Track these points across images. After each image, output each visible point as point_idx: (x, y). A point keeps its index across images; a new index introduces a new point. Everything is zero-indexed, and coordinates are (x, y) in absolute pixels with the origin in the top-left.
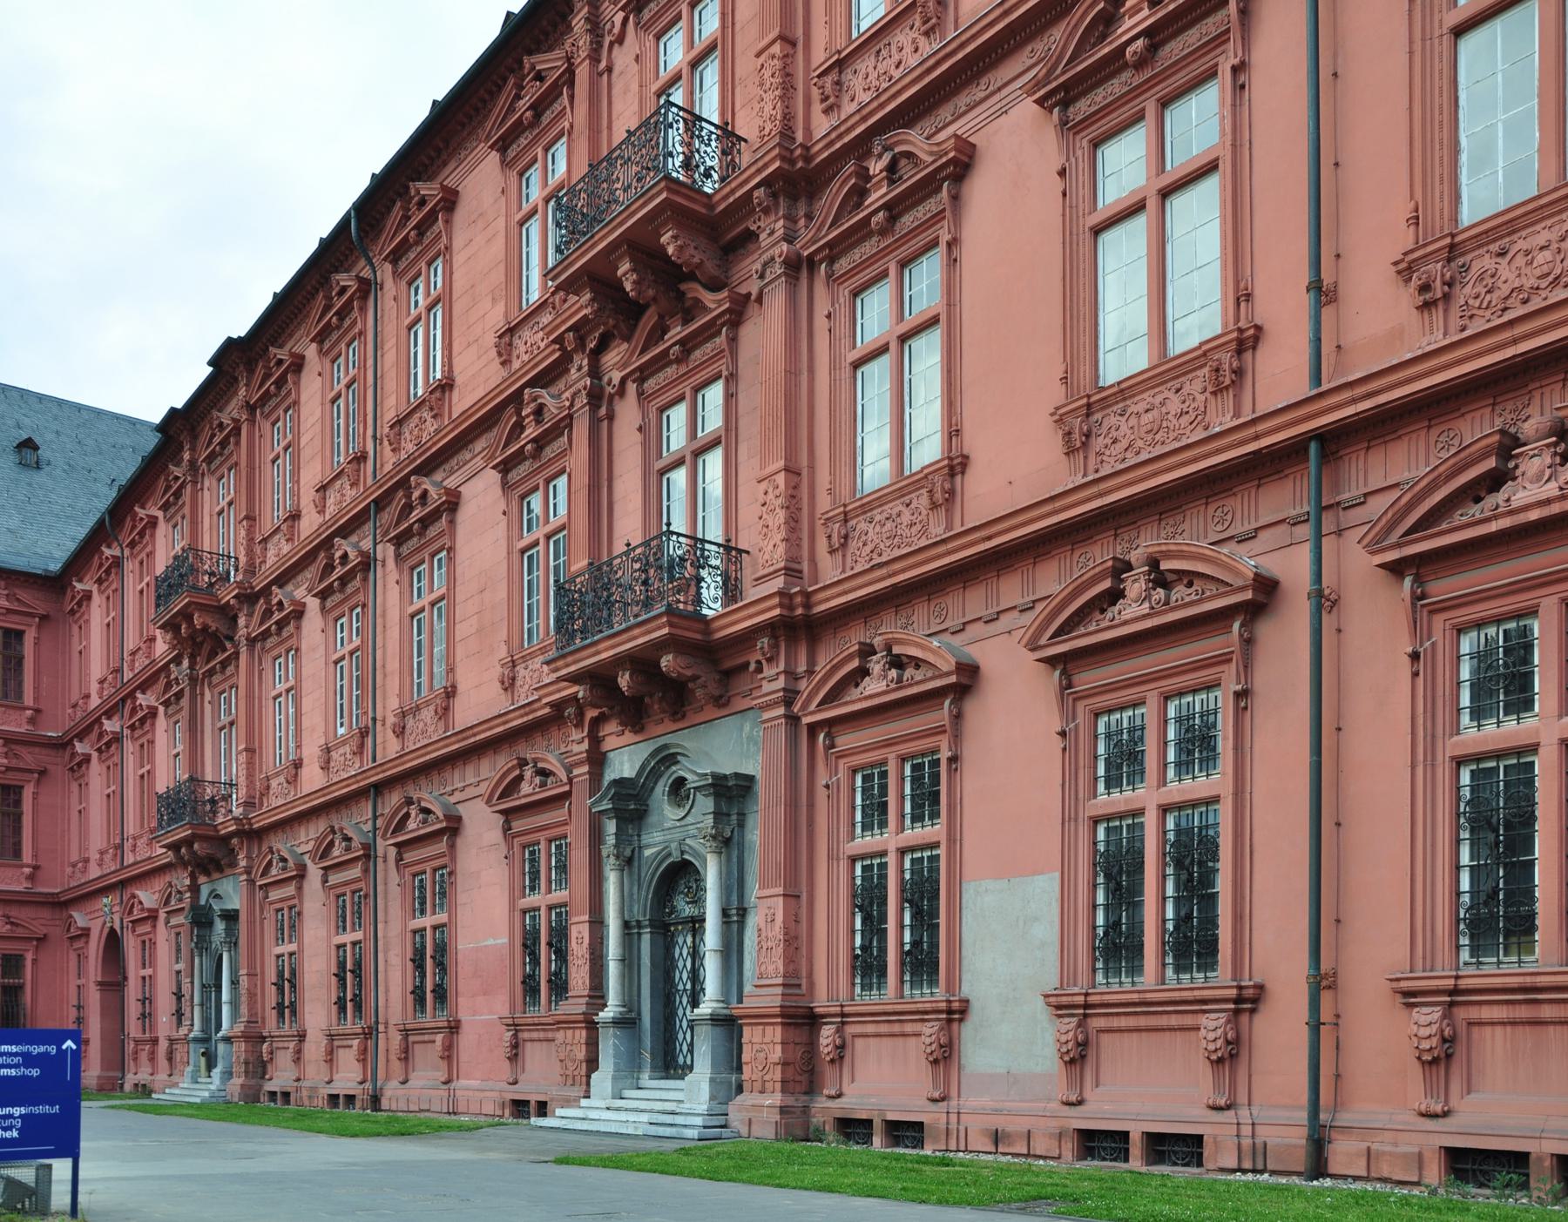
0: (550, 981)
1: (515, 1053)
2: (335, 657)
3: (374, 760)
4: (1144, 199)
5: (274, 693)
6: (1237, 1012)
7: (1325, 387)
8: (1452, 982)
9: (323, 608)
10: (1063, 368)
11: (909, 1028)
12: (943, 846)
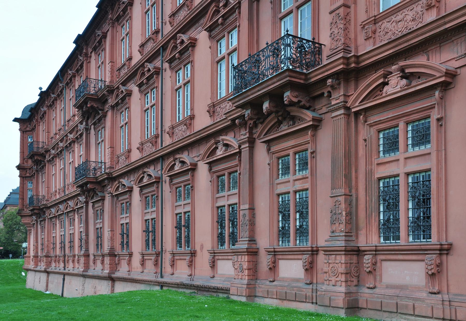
0: (230, 236)
1: (213, 265)
2: (145, 109)
3: (162, 146)
4: (292, 10)
5: (121, 125)
6: (312, 254)
7: (163, 146)
8: (375, 248)
9: (140, 91)
10: (365, 7)
11: (230, 257)
12: (310, 189)
